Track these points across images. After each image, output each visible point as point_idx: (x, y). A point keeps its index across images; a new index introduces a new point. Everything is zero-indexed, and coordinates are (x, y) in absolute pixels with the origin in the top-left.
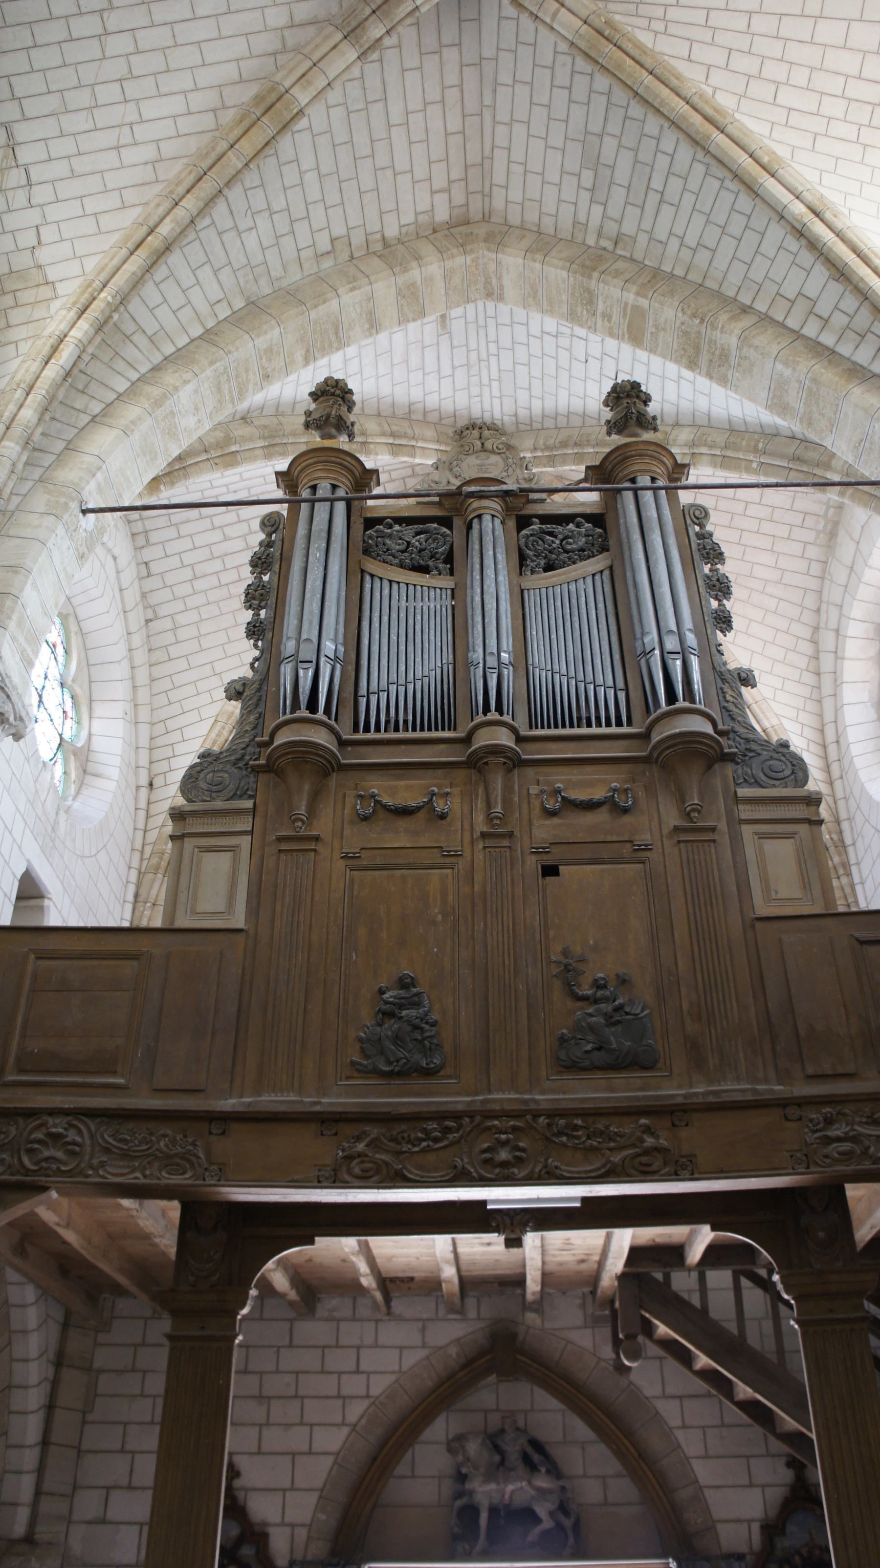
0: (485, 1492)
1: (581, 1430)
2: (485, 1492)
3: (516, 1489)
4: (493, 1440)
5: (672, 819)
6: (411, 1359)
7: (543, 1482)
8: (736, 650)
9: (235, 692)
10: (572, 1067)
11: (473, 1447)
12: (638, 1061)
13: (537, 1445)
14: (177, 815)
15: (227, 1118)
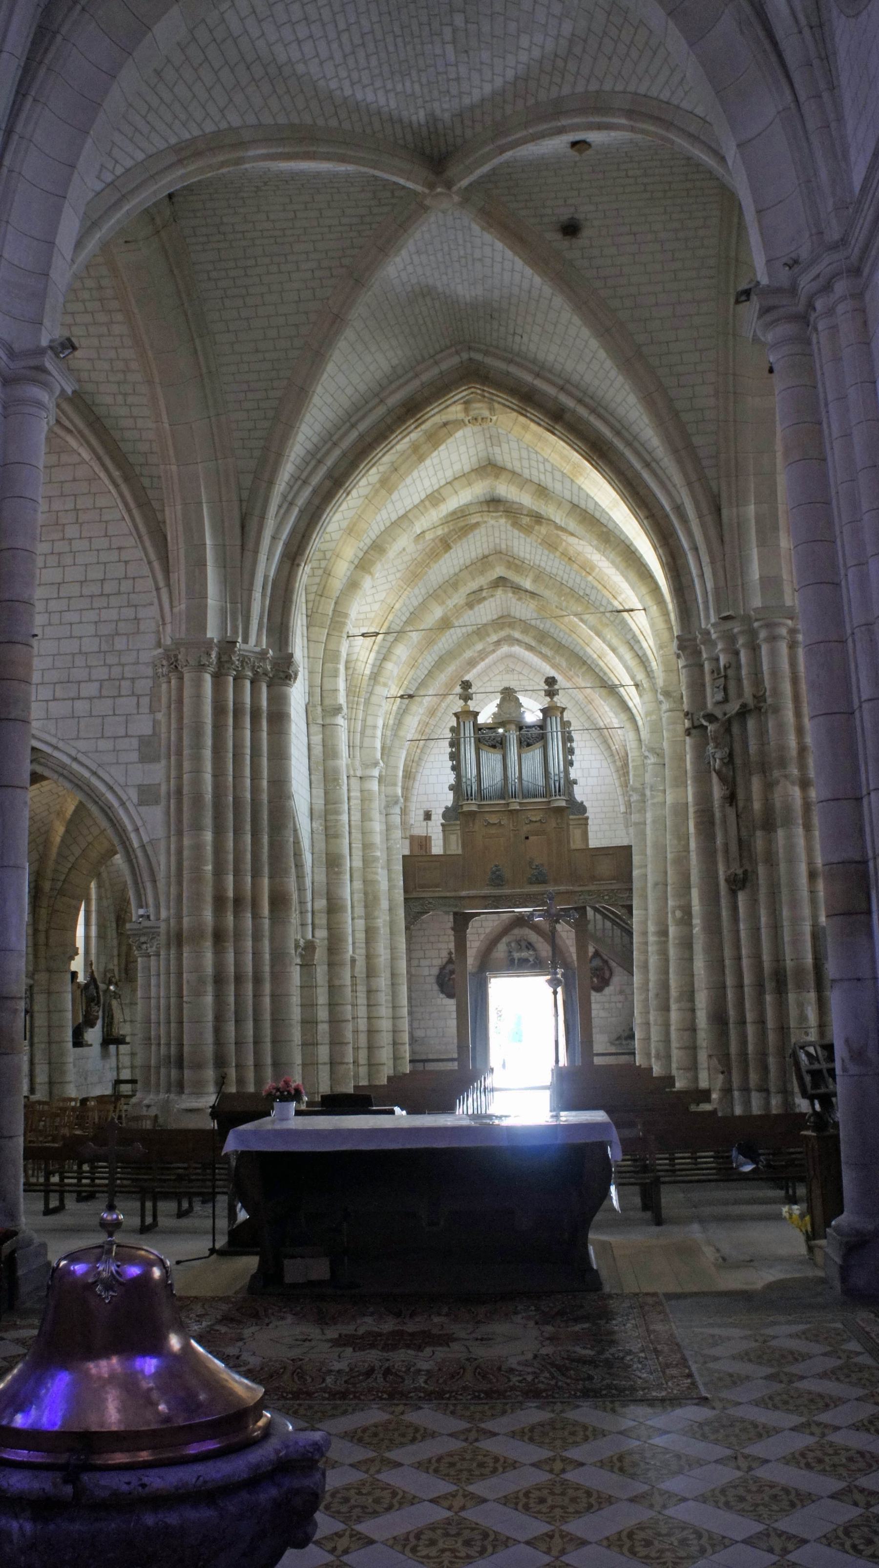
0: (516, 955)
1: (541, 939)
2: (516, 955)
3: (524, 954)
4: (518, 942)
5: (554, 825)
6: (496, 923)
7: (531, 952)
8: (573, 774)
9: (451, 788)
10: (531, 883)
11: (513, 945)
12: (544, 882)
13: (530, 944)
14: (442, 825)
15: (464, 898)
